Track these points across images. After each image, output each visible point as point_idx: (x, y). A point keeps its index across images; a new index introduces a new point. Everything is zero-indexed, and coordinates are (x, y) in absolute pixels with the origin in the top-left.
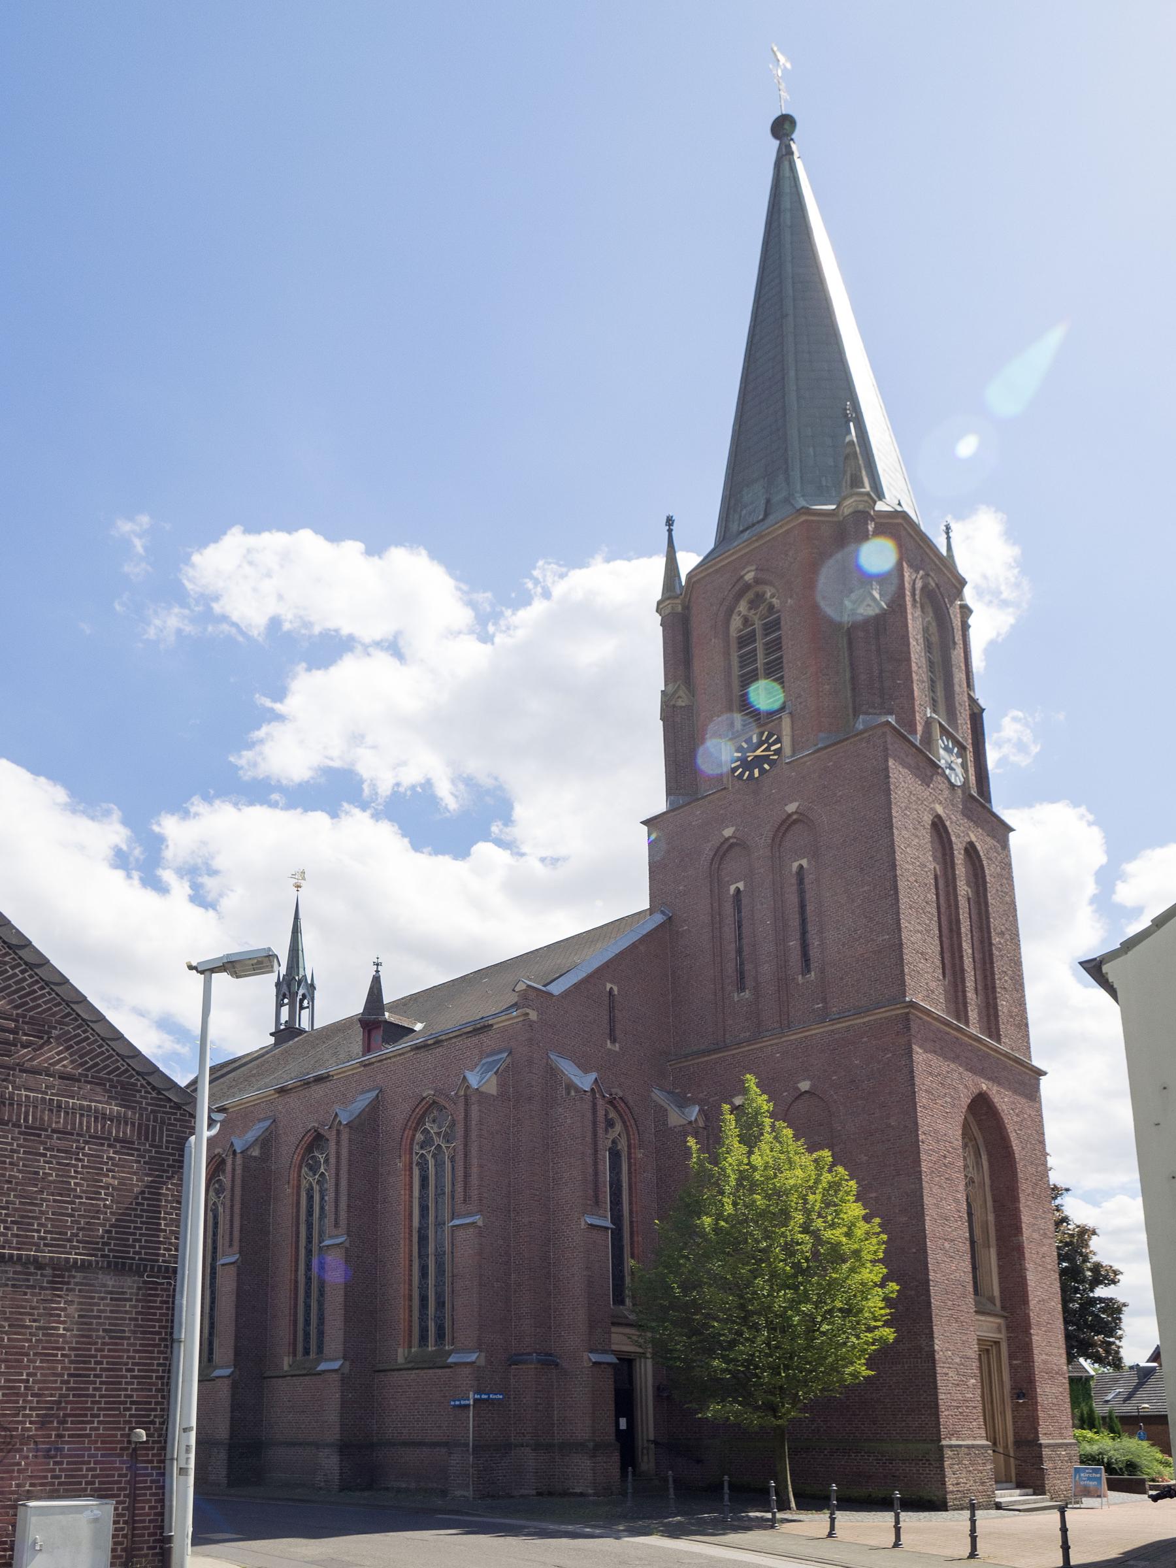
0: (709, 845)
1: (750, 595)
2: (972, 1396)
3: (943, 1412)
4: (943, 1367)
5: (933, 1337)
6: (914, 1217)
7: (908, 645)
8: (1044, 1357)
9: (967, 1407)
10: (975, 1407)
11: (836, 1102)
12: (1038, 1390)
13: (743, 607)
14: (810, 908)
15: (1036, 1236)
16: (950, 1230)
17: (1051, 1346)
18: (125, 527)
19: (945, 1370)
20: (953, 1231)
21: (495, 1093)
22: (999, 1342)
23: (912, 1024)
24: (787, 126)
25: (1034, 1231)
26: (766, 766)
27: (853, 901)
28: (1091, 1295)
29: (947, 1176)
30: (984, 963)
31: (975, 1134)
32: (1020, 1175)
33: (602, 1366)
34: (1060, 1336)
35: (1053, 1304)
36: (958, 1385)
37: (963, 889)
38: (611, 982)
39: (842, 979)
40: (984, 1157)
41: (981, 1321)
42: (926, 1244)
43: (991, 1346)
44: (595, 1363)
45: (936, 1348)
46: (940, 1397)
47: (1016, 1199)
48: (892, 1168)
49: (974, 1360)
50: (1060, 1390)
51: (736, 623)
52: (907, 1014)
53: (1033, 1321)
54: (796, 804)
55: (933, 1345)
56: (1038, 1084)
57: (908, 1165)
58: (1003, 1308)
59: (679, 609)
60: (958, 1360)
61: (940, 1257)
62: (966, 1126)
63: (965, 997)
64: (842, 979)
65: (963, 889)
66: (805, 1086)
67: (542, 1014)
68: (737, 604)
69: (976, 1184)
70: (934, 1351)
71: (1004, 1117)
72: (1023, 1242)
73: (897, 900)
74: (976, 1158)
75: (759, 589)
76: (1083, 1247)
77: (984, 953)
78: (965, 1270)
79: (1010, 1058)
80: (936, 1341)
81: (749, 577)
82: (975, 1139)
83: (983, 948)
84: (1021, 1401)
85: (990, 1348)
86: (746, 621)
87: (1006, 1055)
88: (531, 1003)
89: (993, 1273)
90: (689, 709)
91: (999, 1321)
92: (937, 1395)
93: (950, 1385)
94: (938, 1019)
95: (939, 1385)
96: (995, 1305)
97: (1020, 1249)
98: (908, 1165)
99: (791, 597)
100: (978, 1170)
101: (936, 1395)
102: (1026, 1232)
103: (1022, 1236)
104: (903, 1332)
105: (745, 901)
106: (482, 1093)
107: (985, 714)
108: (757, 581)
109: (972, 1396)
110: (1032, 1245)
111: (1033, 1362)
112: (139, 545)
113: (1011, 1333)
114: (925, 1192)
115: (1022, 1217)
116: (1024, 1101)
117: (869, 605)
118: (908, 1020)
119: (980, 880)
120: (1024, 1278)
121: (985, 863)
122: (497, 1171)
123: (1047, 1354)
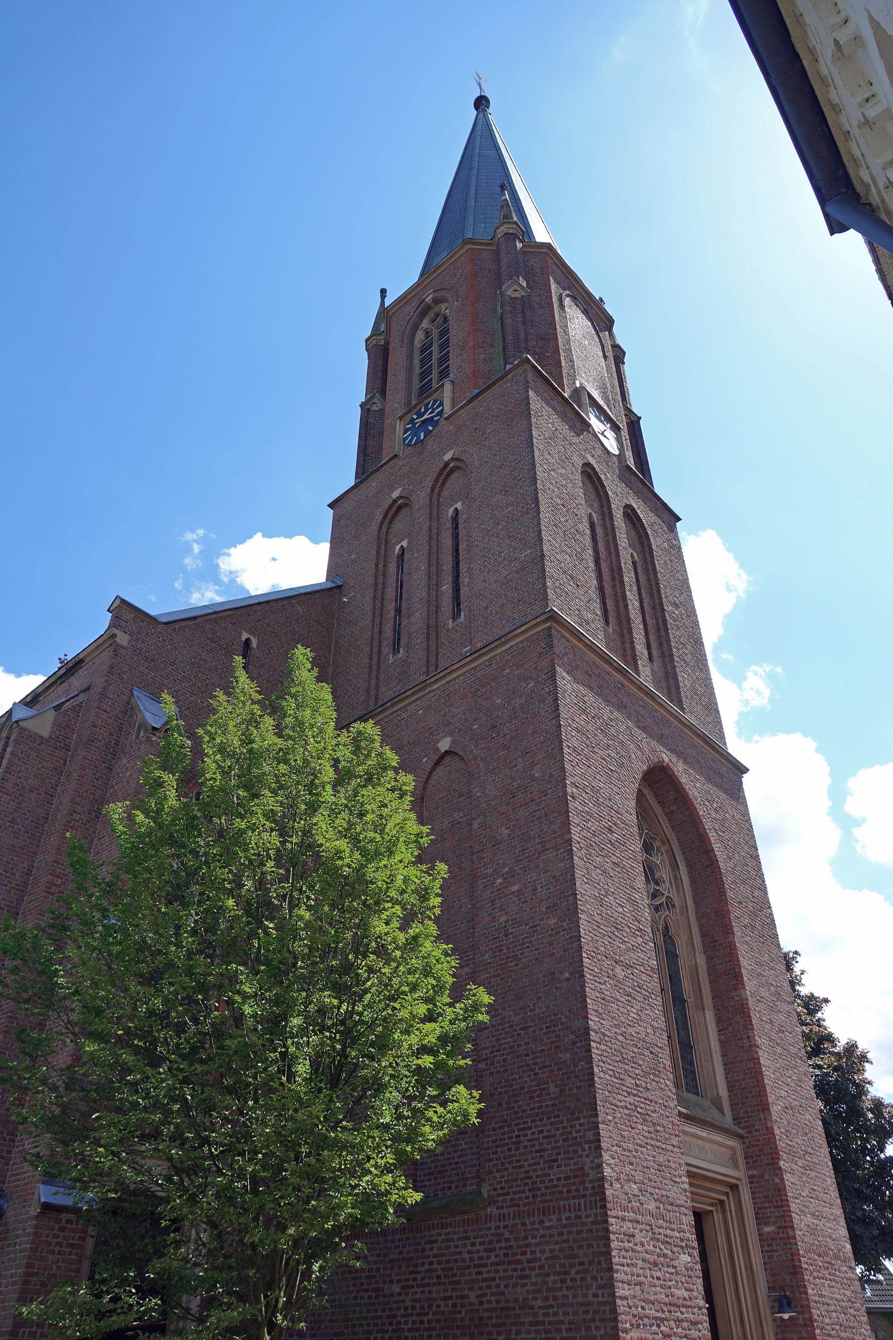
0: (381, 509)
1: (431, 314)
2: (686, 1294)
3: (626, 1331)
4: (623, 1219)
5: (599, 1147)
6: (566, 916)
7: (556, 329)
8: (809, 1219)
9: (678, 1321)
10: (695, 1323)
11: (475, 759)
12: (810, 1291)
13: (425, 324)
14: (462, 547)
15: (764, 992)
16: (623, 947)
17: (817, 1198)
18: (189, 536)
19: (627, 1226)
20: (628, 949)
21: (46, 735)
22: (737, 1186)
23: (555, 641)
24: (484, 102)
25: (760, 985)
26: (430, 428)
27: (498, 524)
28: (882, 1156)
29: (615, 860)
30: (659, 629)
31: (667, 832)
32: (730, 894)
33: (64, 1216)
34: (829, 1181)
35: (808, 1117)
36: (655, 1264)
37: (626, 552)
38: (249, 631)
39: (486, 608)
40: (683, 868)
41: (701, 1138)
42: (582, 961)
43: (727, 1194)
44: (47, 1207)
45: (607, 1171)
46: (619, 1292)
47: (728, 930)
48: (537, 841)
49: (682, 1209)
50: (848, 1293)
51: (420, 336)
52: (550, 628)
53: (781, 1144)
54: (452, 452)
55: (599, 1166)
56: (741, 783)
57: (555, 833)
58: (736, 1119)
59: (383, 343)
60: (652, 1206)
61: (608, 989)
62: (640, 796)
63: (633, 648)
64: (486, 608)
65: (626, 552)
66: (444, 745)
67: (137, 640)
68: (421, 322)
69: (678, 909)
70: (602, 1179)
71: (697, 806)
72: (747, 1000)
73: (538, 512)
74: (673, 870)
75: (436, 309)
76: (855, 1073)
77: (657, 619)
78: (656, 1025)
79: (698, 735)
80: (606, 1157)
81: (429, 299)
82: (669, 842)
83: (655, 613)
84: (786, 1316)
85: (724, 1198)
86: (428, 333)
87: (690, 727)
88: (123, 624)
89: (714, 1054)
90: (382, 412)
91: (731, 1143)
92: (612, 1286)
93: (640, 1262)
94: (592, 648)
95: (615, 1260)
96: (723, 1113)
97: (743, 1009)
98: (555, 833)
99: (457, 300)
100: (678, 888)
101: (610, 1285)
102: (750, 985)
103: (744, 989)
104: (557, 1142)
105: (406, 556)
106: (24, 729)
107: (642, 423)
108: (436, 301)
109: (686, 1294)
110: (761, 1007)
111: (793, 1227)
112: (196, 548)
113: (753, 1168)
114: (578, 873)
115: (741, 959)
116: (724, 796)
117: (516, 290)
118: (550, 636)
119: (647, 548)
120: (756, 1061)
121: (649, 532)
122: (13, 845)
123: (813, 1215)
